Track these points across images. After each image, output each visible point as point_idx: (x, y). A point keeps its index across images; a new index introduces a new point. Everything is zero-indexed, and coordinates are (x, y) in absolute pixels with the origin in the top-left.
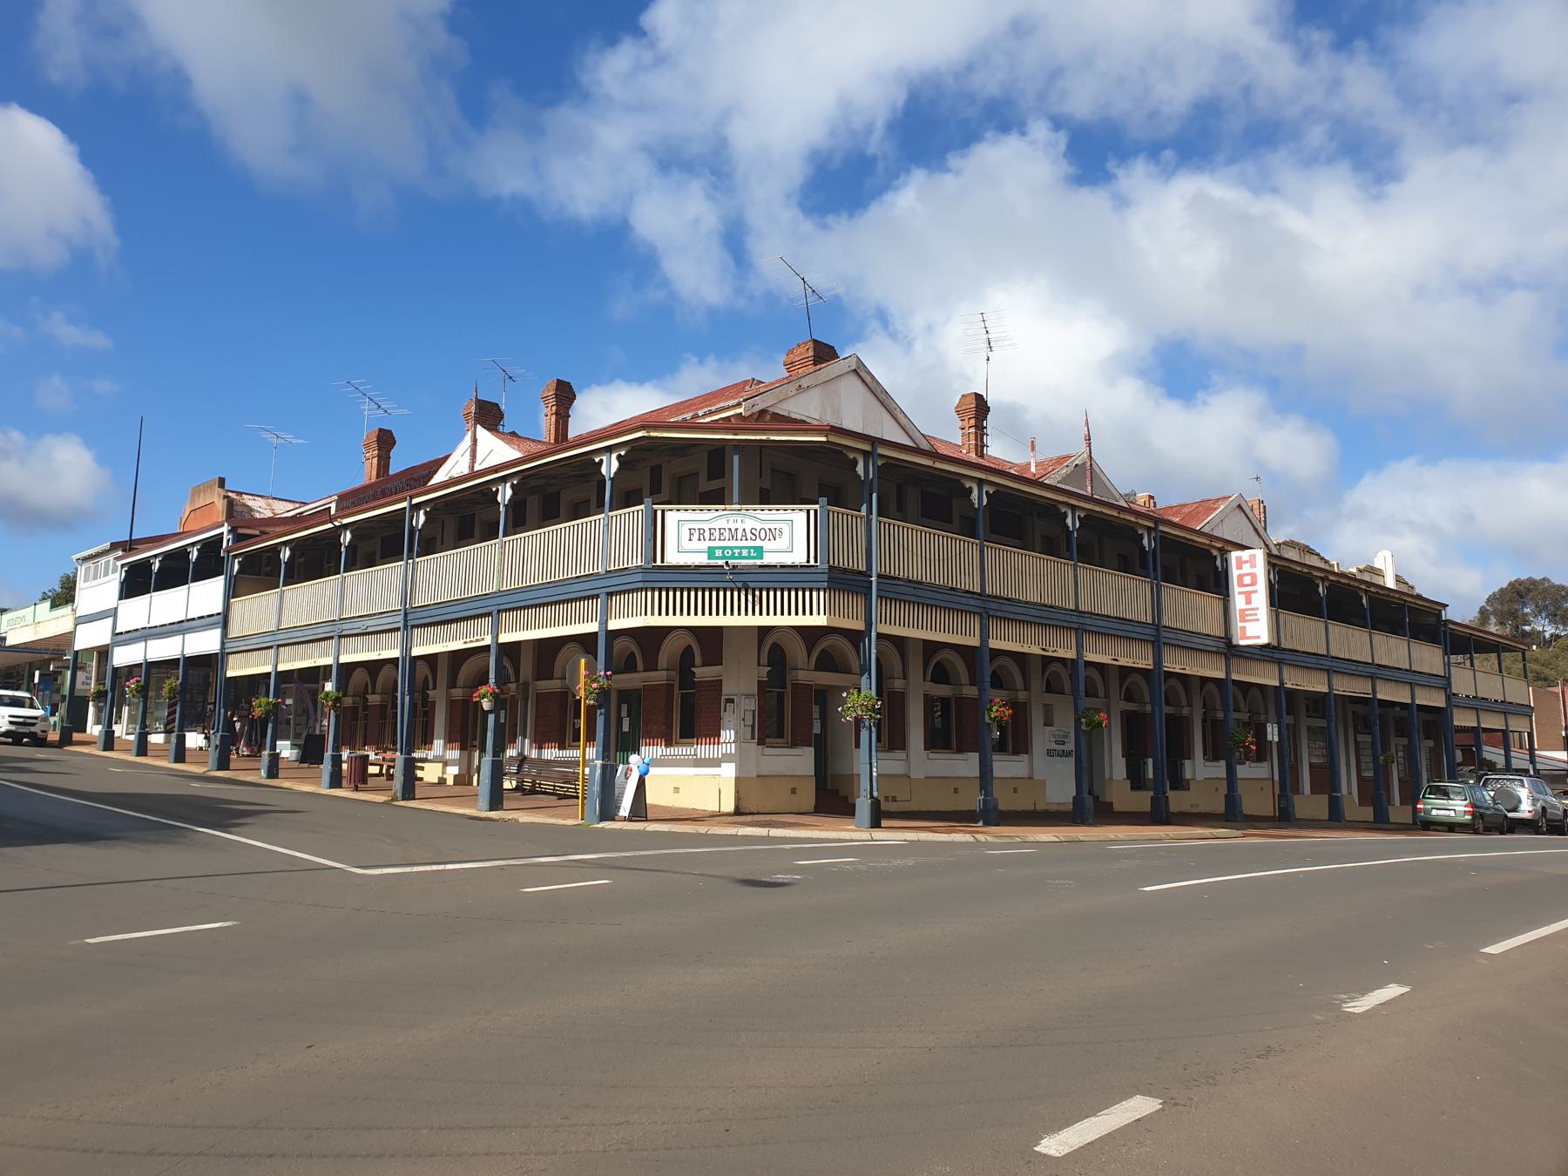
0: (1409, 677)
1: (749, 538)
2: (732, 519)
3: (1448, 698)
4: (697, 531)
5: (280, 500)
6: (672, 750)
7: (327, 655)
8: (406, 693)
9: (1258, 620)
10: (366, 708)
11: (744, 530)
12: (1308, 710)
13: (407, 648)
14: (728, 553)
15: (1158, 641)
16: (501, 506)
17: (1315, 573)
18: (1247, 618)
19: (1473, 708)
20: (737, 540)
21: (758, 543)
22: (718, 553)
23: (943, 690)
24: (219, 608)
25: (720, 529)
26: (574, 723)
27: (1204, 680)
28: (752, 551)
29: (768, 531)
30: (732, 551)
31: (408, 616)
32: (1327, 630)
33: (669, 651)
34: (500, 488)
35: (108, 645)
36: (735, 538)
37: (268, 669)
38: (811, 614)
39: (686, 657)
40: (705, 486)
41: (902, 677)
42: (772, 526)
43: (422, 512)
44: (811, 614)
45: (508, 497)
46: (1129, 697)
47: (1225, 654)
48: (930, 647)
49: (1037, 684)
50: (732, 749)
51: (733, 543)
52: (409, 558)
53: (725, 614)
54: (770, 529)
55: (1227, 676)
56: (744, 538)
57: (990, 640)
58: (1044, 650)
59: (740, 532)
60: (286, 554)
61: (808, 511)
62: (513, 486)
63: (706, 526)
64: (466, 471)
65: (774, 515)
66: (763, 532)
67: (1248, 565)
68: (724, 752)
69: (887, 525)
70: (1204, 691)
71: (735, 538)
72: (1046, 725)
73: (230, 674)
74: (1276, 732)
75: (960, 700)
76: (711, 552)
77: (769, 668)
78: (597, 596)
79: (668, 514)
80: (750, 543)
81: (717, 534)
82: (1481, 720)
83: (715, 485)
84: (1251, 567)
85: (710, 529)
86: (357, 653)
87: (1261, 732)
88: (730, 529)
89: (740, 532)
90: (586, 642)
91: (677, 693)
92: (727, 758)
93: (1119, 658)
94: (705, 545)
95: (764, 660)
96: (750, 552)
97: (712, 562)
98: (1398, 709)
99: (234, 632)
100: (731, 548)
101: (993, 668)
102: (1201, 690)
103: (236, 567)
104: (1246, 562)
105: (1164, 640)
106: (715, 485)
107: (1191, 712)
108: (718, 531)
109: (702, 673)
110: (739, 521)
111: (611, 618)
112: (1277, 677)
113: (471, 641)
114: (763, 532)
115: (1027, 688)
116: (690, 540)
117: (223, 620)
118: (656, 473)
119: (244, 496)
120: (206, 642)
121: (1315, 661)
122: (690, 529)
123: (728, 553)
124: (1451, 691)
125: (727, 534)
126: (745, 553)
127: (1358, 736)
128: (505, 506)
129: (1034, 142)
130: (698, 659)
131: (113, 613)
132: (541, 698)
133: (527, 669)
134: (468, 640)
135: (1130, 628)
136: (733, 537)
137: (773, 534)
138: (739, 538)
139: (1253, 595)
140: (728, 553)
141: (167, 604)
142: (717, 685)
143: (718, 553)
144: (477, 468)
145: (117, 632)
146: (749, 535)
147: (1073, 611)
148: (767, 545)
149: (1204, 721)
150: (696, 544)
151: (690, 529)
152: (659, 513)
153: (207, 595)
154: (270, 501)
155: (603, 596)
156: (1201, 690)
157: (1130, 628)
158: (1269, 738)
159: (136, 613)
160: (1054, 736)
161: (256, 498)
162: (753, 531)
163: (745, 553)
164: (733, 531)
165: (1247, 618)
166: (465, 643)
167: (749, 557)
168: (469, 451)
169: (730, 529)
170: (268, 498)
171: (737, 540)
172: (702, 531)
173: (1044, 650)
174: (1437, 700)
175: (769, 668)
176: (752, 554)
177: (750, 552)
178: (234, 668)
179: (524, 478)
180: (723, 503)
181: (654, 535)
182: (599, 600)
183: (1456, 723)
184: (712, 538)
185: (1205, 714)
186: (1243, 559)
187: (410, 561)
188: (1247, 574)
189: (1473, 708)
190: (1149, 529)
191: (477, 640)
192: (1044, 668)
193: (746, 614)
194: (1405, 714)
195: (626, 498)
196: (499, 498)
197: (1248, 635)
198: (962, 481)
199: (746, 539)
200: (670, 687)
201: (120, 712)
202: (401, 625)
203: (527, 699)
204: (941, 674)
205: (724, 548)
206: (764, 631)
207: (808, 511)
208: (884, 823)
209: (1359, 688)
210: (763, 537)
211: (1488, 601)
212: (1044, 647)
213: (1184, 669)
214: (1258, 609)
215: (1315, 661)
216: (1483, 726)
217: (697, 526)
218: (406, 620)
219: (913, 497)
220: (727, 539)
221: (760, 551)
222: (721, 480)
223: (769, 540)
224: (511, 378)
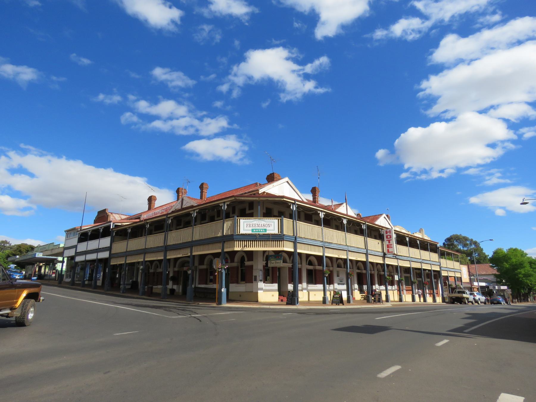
2: (258, 221)
3: (440, 268)
5: (123, 215)
7: (141, 259)
10: (149, 272)
13: (165, 256)
18: (389, 247)
21: (265, 228)
22: (254, 230)
24: (109, 245)
27: (377, 264)
33: (237, 258)
35: (108, 258)
37: (123, 262)
38: (280, 247)
39: (242, 260)
42: (269, 223)
44: (280, 247)
46: (358, 269)
48: (308, 256)
49: (335, 265)
50: (383, 287)
51: (258, 228)
53: (254, 247)
55: (347, 257)
57: (325, 254)
58: (339, 256)
59: (260, 225)
61: (279, 220)
63: (251, 223)
70: (337, 263)
72: (337, 276)
73: (112, 264)
74: (397, 278)
75: (315, 270)
77: (266, 262)
79: (241, 220)
80: (263, 228)
81: (254, 225)
83: (251, 211)
84: (390, 233)
86: (150, 258)
89: (260, 225)
91: (240, 269)
94: (251, 228)
95: (265, 259)
96: (263, 230)
98: (427, 271)
99: (113, 251)
100: (258, 229)
101: (337, 263)
102: (336, 262)
103: (114, 234)
104: (388, 232)
105: (298, 241)
106: (251, 211)
108: (254, 225)
109: (247, 263)
113: (184, 255)
115: (332, 267)
119: (113, 214)
120: (105, 255)
125: (257, 225)
126: (261, 231)
127: (417, 278)
130: (246, 259)
131: (76, 247)
132: (201, 270)
133: (196, 263)
137: (269, 225)
139: (391, 241)
141: (93, 244)
142: (251, 267)
143: (254, 230)
144: (184, 206)
145: (77, 252)
146: (263, 226)
148: (267, 228)
149: (378, 275)
152: (238, 220)
153: (105, 242)
154: (120, 215)
156: (336, 262)
158: (396, 279)
159: (82, 247)
160: (340, 279)
163: (261, 231)
164: (258, 224)
165: (389, 247)
166: (182, 255)
167: (263, 232)
173: (338, 256)
177: (263, 230)
181: (235, 226)
183: (443, 275)
185: (378, 273)
186: (388, 231)
188: (389, 235)
190: (364, 224)
191: (186, 254)
192: (337, 261)
194: (430, 272)
200: (237, 267)
201: (425, 287)
203: (197, 271)
205: (256, 229)
207: (279, 220)
208: (333, 304)
209: (417, 266)
211: (445, 240)
214: (392, 244)
215: (416, 260)
216: (449, 275)
217: (248, 223)
221: (266, 230)
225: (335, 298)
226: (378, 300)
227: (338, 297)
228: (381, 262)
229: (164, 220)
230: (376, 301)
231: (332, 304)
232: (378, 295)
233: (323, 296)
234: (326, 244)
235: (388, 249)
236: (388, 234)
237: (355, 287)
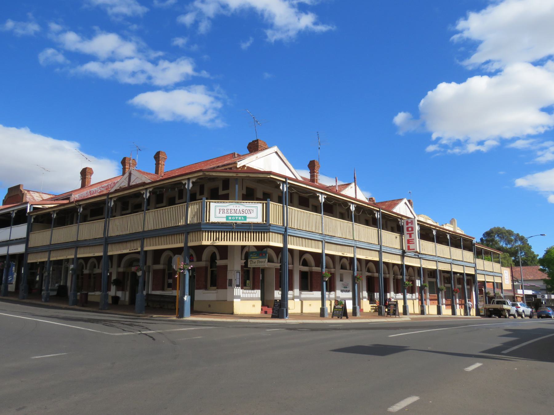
0: (436, 259)
1: (241, 213)
2: (235, 206)
3: (476, 271)
4: (222, 210)
6: (254, 291)
9: (414, 243)
10: (82, 274)
11: (240, 210)
12: (428, 275)
13: (105, 251)
14: (234, 218)
15: (381, 250)
16: (145, 199)
17: (432, 227)
18: (410, 243)
19: (483, 274)
20: (237, 213)
21: (245, 215)
22: (230, 218)
23: (305, 269)
24: (25, 235)
25: (230, 209)
26: (168, 281)
27: (394, 265)
28: (242, 218)
29: (248, 210)
30: (235, 218)
32: (450, 250)
36: (236, 213)
37: (46, 259)
38: (264, 241)
40: (221, 192)
41: (333, 268)
42: (250, 209)
44: (264, 241)
46: (369, 271)
47: (283, 234)
48: (302, 253)
49: (338, 266)
54: (249, 210)
56: (239, 213)
57: (325, 250)
58: (367, 258)
59: (238, 211)
63: (225, 208)
64: (127, 186)
65: (251, 205)
66: (246, 211)
67: (410, 224)
69: (279, 206)
71: (236, 213)
73: (29, 261)
74: (419, 283)
75: (311, 272)
76: (227, 218)
77: (245, 261)
79: (211, 204)
80: (241, 215)
81: (229, 211)
82: (486, 278)
83: (225, 192)
85: (227, 209)
87: (414, 282)
88: (234, 209)
89: (238, 211)
90: (177, 251)
91: (209, 270)
93: (367, 257)
94: (225, 215)
96: (241, 218)
97: (228, 221)
98: (458, 275)
100: (235, 216)
103: (32, 220)
104: (410, 223)
105: (289, 234)
106: (225, 192)
107: (293, 267)
109: (220, 262)
110: (238, 206)
111: (189, 242)
112: (420, 263)
114: (246, 211)
116: (220, 213)
117: (26, 241)
118: (202, 188)
120: (20, 249)
121: (432, 258)
122: (219, 209)
123: (233, 218)
124: (476, 268)
125: (233, 211)
126: (240, 218)
127: (445, 284)
128: (146, 199)
130: (218, 257)
132: (155, 272)
133: (149, 261)
134: (131, 249)
135: (372, 246)
136: (235, 212)
137: (250, 212)
138: (238, 213)
139: (412, 235)
140: (233, 218)
142: (225, 267)
143: (230, 218)
144: (132, 183)
147: (352, 240)
148: (248, 215)
149: (394, 279)
150: (221, 215)
151: (219, 209)
152: (208, 203)
153: (20, 231)
156: (393, 268)
157: (372, 246)
161: (35, 193)
162: (243, 210)
163: (240, 218)
164: (235, 210)
165: (410, 243)
166: (130, 250)
167: (232, 220)
168: (128, 177)
169: (234, 209)
170: (40, 193)
171: (237, 213)
172: (224, 210)
173: (343, 254)
174: (471, 271)
175: (245, 261)
176: (242, 219)
177: (241, 218)
179: (154, 189)
180: (228, 200)
183: (478, 279)
184: (231, 213)
185: (394, 277)
187: (108, 219)
189: (483, 274)
190: (377, 211)
193: (238, 241)
194: (461, 277)
195: (193, 198)
197: (410, 248)
198: (276, 181)
199: (240, 213)
200: (206, 268)
204: (305, 263)
205: (232, 217)
206: (243, 247)
207: (263, 204)
209: (446, 267)
210: (246, 212)
212: (343, 253)
213: (389, 261)
219: (296, 199)
220: (233, 213)
222: (228, 190)
223: (249, 214)
224: (140, 149)
227: (341, 307)
230: (390, 313)
232: (393, 306)
235: (409, 245)
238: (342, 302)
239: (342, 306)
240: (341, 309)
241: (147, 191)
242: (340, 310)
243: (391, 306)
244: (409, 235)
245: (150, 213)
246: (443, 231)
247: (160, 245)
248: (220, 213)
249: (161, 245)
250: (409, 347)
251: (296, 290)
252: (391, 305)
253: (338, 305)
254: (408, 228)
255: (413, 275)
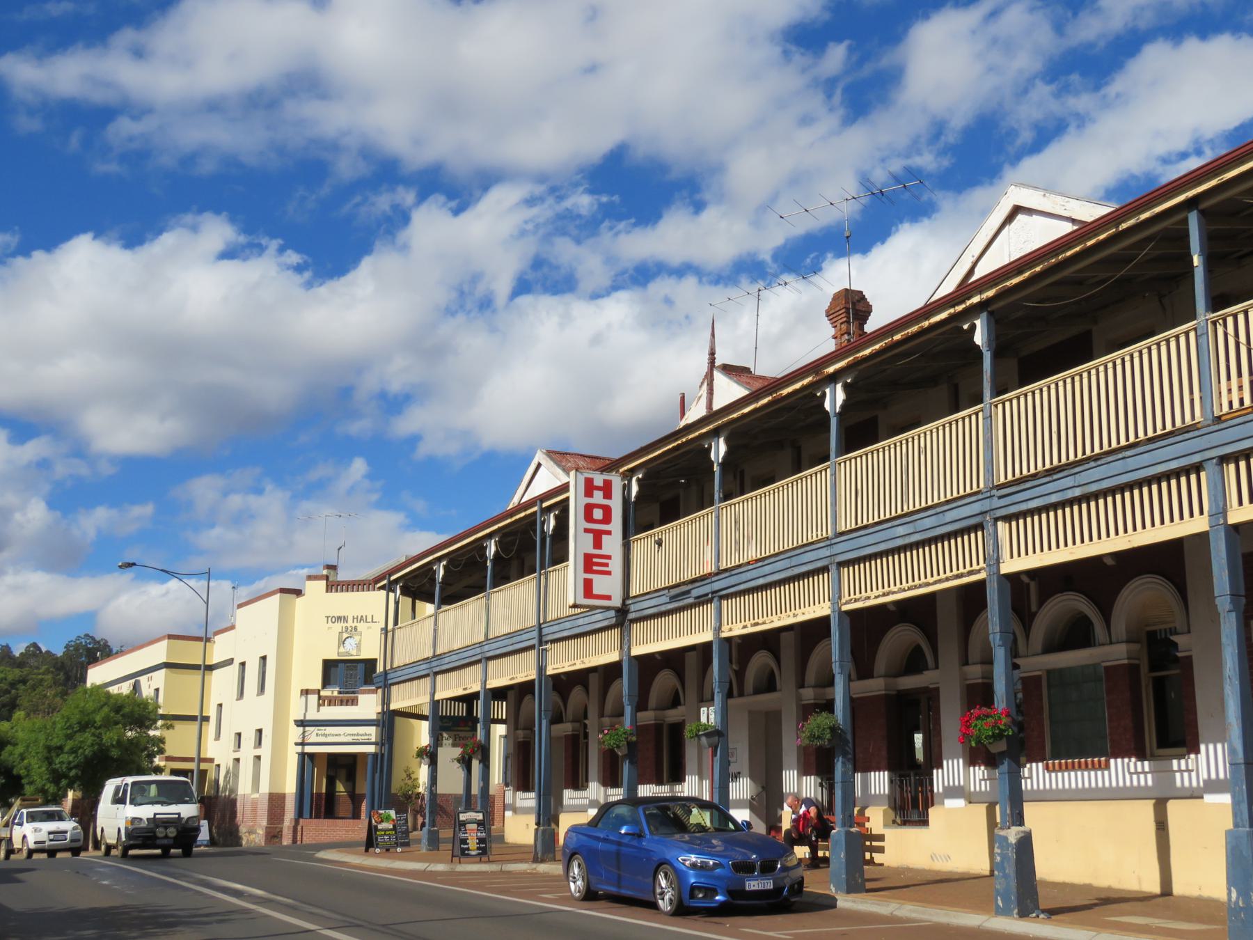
8: (543, 716)
16: (715, 465)
18: (595, 568)
31: (543, 630)
34: (828, 391)
43: (839, 387)
45: (839, 401)
52: (541, 569)
60: (492, 549)
62: (846, 388)
68: (946, 784)
78: (1197, 468)
92: (1213, 786)
121: (653, 602)
128: (719, 465)
129: (1024, 90)
134: (881, 591)
139: (605, 537)
155: (833, 569)
165: (595, 568)
178: (442, 690)
182: (1203, 475)
196: (827, 406)
202: (535, 642)
214: (609, 557)
218: (541, 636)
225: (383, 833)
226: (478, 848)
227: (391, 827)
228: (990, 632)
229: (530, 522)
230: (468, 849)
231: (367, 850)
232: (474, 826)
233: (1230, 826)
234: (837, 549)
235: (589, 576)
236: (598, 497)
237: (874, 790)
238: (389, 815)
239: (392, 823)
240: (390, 830)
241: (718, 441)
242: (391, 832)
243: (469, 826)
244: (591, 536)
245: (700, 521)
246: (899, 343)
247: (647, 643)
248: (220, 705)
249: (661, 640)
250: (119, 830)
251: (872, 773)
252: (467, 825)
253: (382, 821)
254: (589, 509)
255: (1179, 624)
